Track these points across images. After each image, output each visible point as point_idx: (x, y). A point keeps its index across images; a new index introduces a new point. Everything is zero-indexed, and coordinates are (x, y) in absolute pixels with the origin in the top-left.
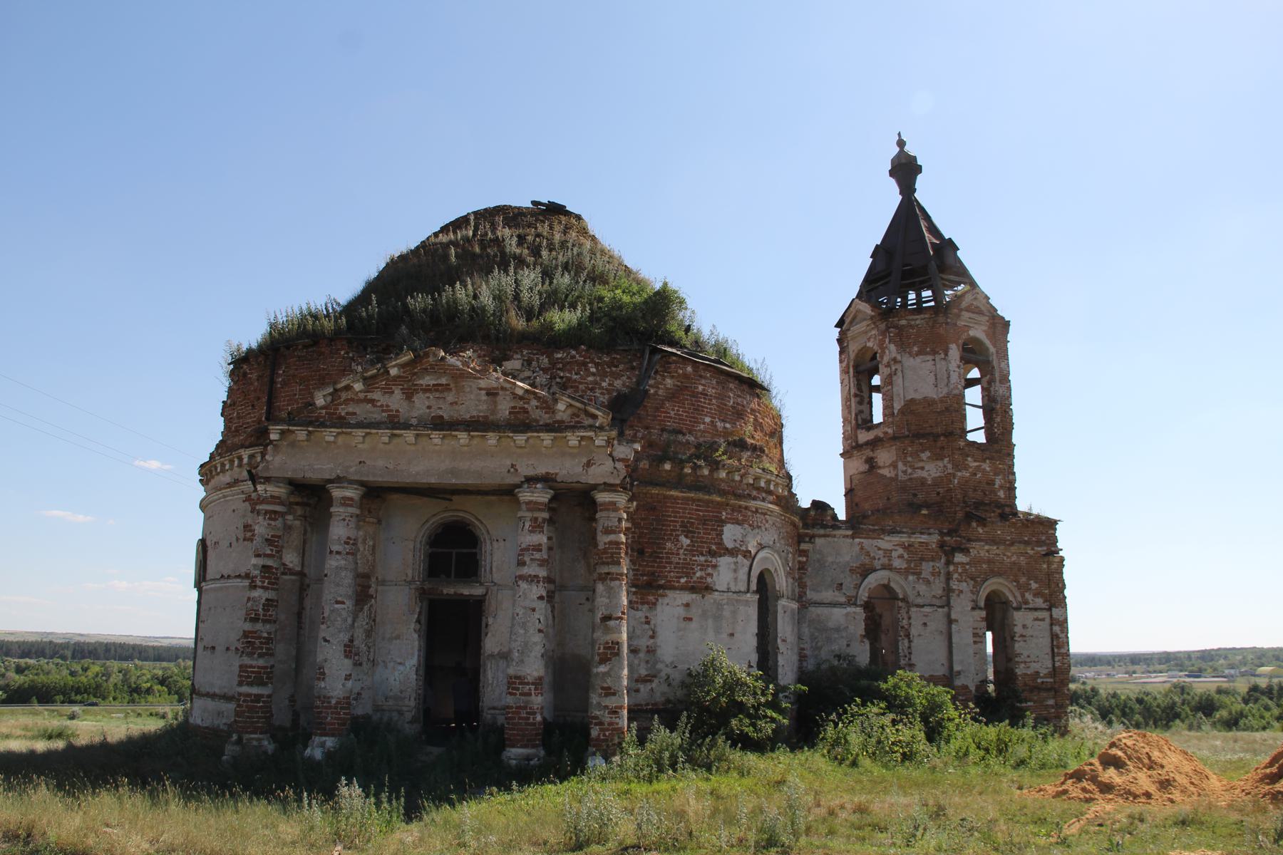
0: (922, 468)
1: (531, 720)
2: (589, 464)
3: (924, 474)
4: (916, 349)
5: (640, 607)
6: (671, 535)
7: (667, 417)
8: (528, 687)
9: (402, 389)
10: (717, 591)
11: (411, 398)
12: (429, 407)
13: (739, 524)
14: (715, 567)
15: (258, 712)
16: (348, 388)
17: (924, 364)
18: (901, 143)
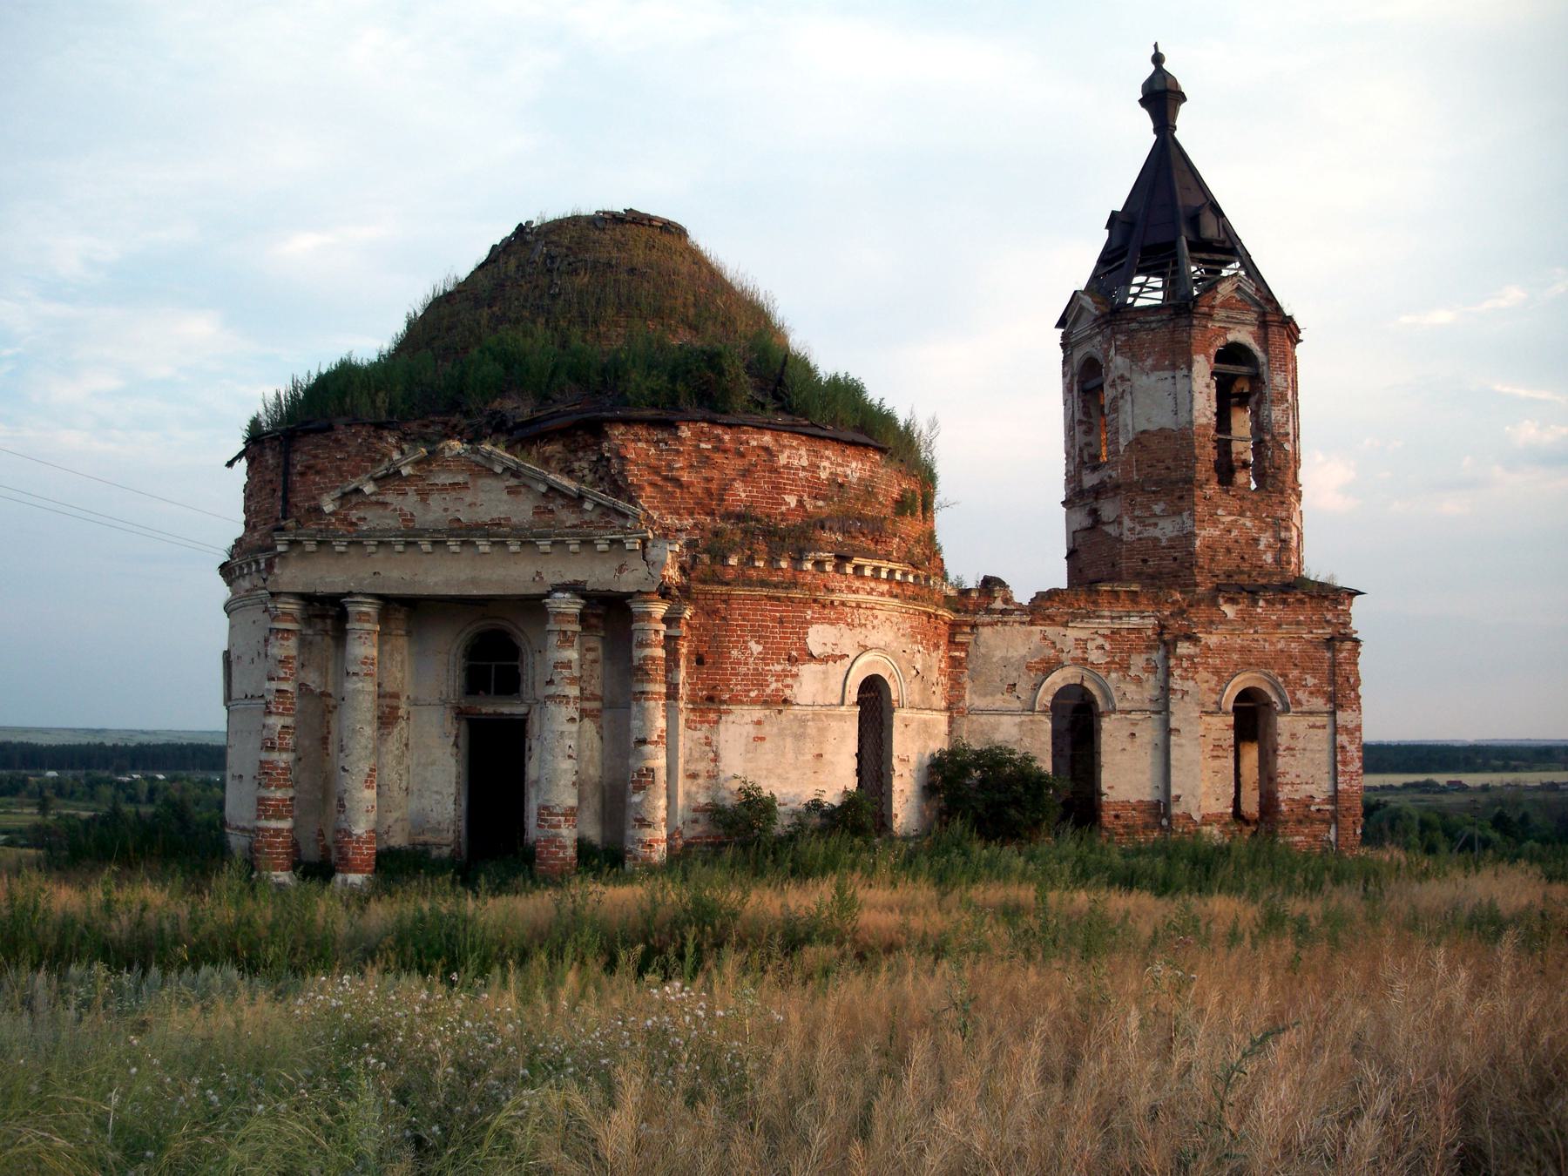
0: (1156, 525)
1: (561, 855)
2: (621, 569)
3: (1157, 533)
4: (1149, 362)
5: (699, 726)
6: (738, 642)
7: (738, 501)
8: (557, 819)
9: (415, 490)
10: (798, 704)
11: (427, 499)
12: (446, 510)
13: (832, 624)
14: (795, 676)
15: (278, 848)
16: (358, 491)
17: (1160, 383)
18: (1158, 59)
